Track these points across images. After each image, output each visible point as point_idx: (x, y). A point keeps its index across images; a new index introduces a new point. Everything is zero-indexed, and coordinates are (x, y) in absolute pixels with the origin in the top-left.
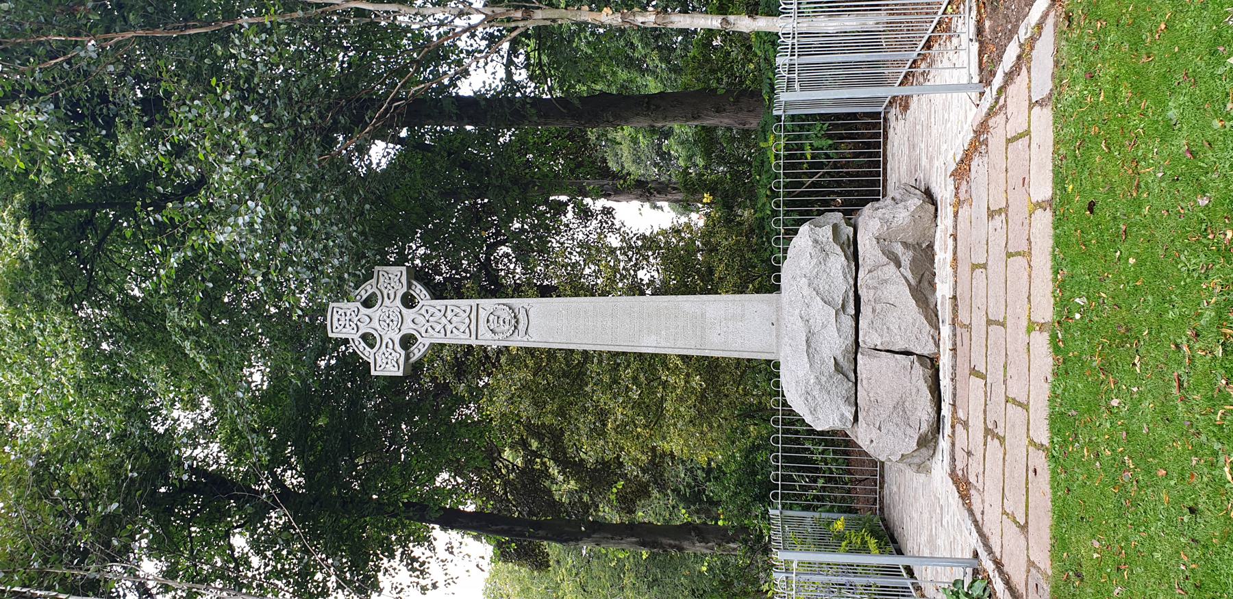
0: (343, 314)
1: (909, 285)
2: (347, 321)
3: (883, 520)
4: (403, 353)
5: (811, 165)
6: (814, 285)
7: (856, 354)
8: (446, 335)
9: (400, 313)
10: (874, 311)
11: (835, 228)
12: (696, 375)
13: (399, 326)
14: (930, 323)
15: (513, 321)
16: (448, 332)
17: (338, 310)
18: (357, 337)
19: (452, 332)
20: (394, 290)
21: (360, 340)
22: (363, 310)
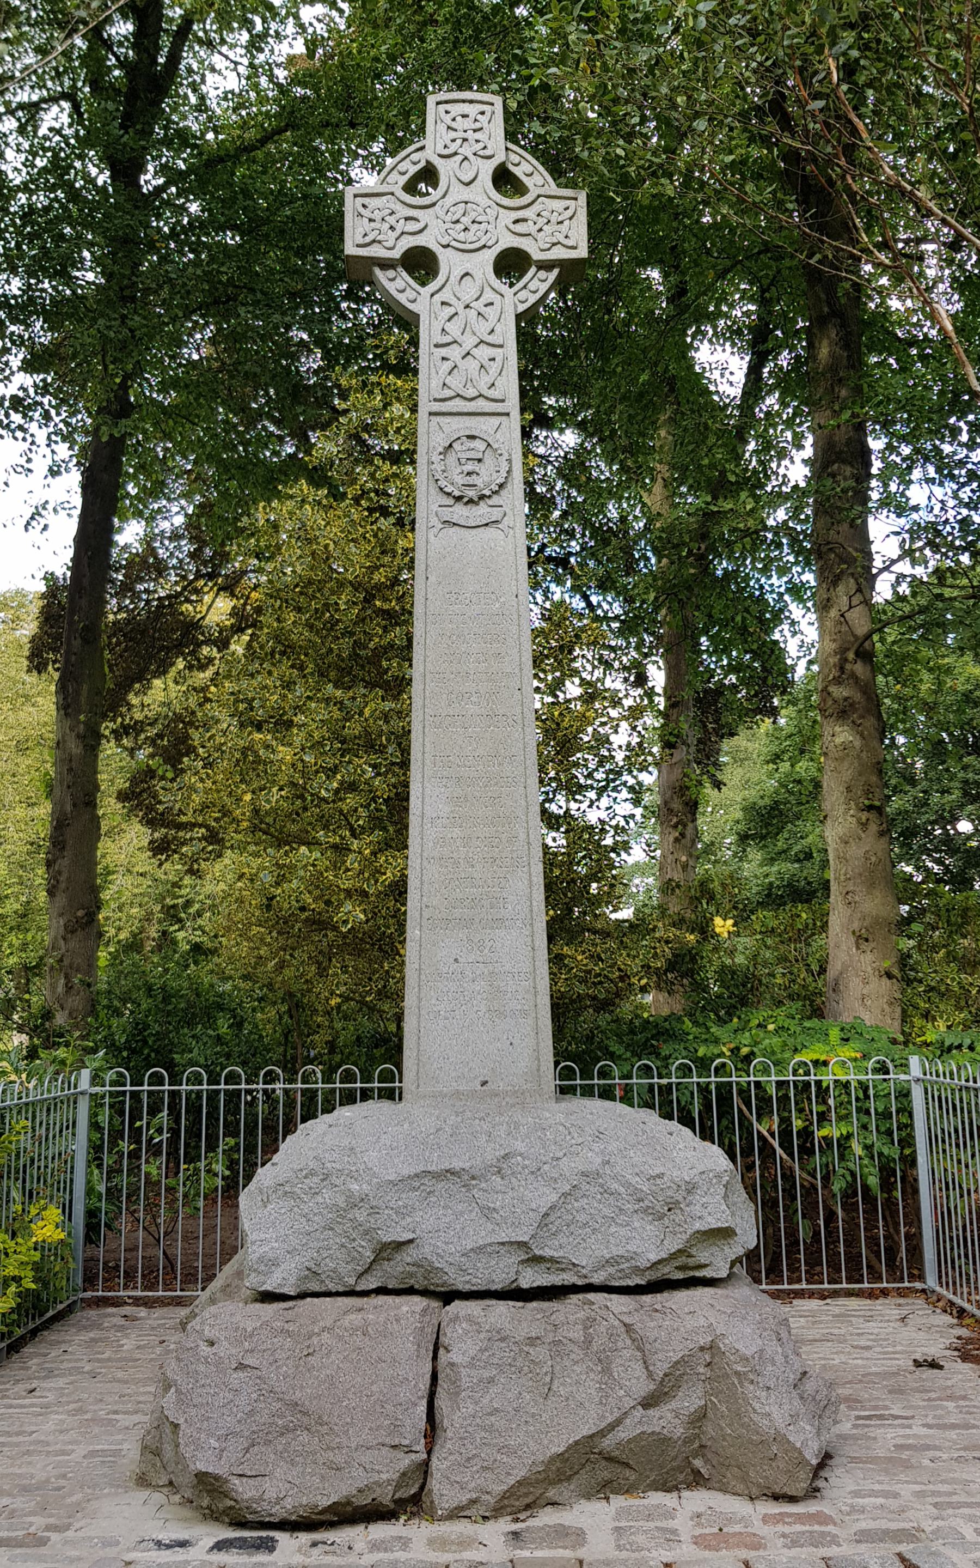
0: (478, 125)
1: (602, 1433)
2: (461, 134)
3: (70, 1309)
4: (397, 254)
5: (806, 1134)
6: (584, 1186)
7: (425, 1293)
8: (436, 346)
9: (484, 246)
10: (533, 1341)
11: (725, 1233)
12: (364, 911)
13: (454, 243)
14: (509, 1494)
15: (471, 493)
16: (443, 352)
17: (488, 114)
18: (429, 155)
19: (477, 141)
20: (534, 232)
21: (423, 164)
22: (487, 169)
